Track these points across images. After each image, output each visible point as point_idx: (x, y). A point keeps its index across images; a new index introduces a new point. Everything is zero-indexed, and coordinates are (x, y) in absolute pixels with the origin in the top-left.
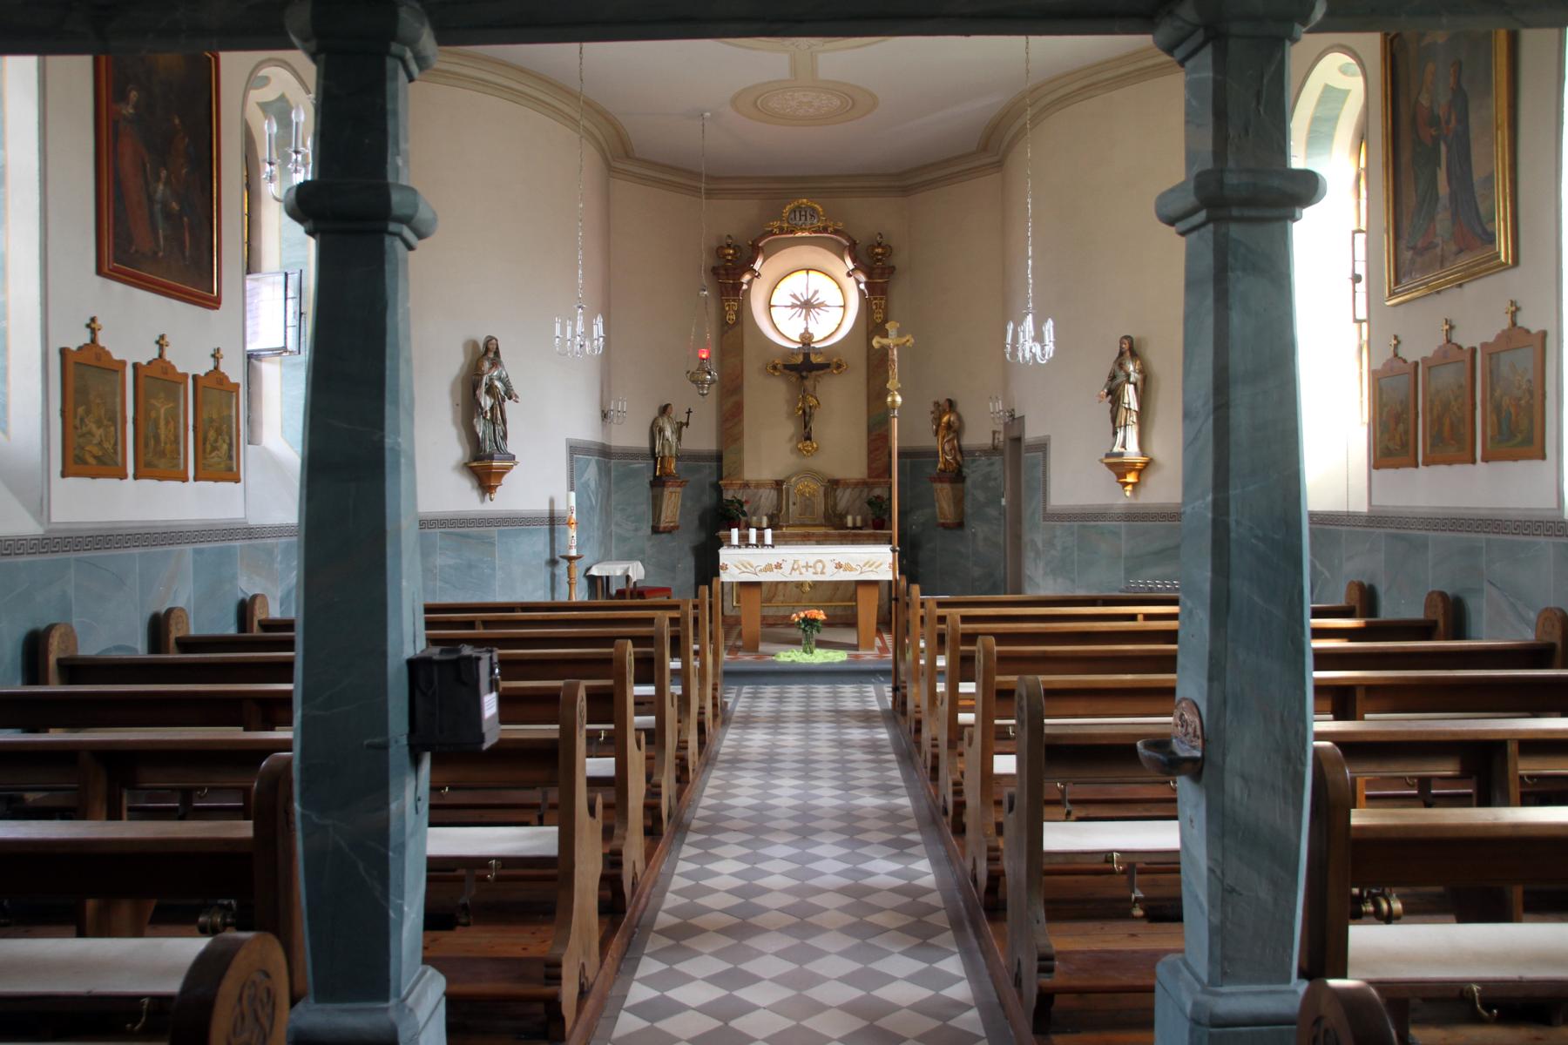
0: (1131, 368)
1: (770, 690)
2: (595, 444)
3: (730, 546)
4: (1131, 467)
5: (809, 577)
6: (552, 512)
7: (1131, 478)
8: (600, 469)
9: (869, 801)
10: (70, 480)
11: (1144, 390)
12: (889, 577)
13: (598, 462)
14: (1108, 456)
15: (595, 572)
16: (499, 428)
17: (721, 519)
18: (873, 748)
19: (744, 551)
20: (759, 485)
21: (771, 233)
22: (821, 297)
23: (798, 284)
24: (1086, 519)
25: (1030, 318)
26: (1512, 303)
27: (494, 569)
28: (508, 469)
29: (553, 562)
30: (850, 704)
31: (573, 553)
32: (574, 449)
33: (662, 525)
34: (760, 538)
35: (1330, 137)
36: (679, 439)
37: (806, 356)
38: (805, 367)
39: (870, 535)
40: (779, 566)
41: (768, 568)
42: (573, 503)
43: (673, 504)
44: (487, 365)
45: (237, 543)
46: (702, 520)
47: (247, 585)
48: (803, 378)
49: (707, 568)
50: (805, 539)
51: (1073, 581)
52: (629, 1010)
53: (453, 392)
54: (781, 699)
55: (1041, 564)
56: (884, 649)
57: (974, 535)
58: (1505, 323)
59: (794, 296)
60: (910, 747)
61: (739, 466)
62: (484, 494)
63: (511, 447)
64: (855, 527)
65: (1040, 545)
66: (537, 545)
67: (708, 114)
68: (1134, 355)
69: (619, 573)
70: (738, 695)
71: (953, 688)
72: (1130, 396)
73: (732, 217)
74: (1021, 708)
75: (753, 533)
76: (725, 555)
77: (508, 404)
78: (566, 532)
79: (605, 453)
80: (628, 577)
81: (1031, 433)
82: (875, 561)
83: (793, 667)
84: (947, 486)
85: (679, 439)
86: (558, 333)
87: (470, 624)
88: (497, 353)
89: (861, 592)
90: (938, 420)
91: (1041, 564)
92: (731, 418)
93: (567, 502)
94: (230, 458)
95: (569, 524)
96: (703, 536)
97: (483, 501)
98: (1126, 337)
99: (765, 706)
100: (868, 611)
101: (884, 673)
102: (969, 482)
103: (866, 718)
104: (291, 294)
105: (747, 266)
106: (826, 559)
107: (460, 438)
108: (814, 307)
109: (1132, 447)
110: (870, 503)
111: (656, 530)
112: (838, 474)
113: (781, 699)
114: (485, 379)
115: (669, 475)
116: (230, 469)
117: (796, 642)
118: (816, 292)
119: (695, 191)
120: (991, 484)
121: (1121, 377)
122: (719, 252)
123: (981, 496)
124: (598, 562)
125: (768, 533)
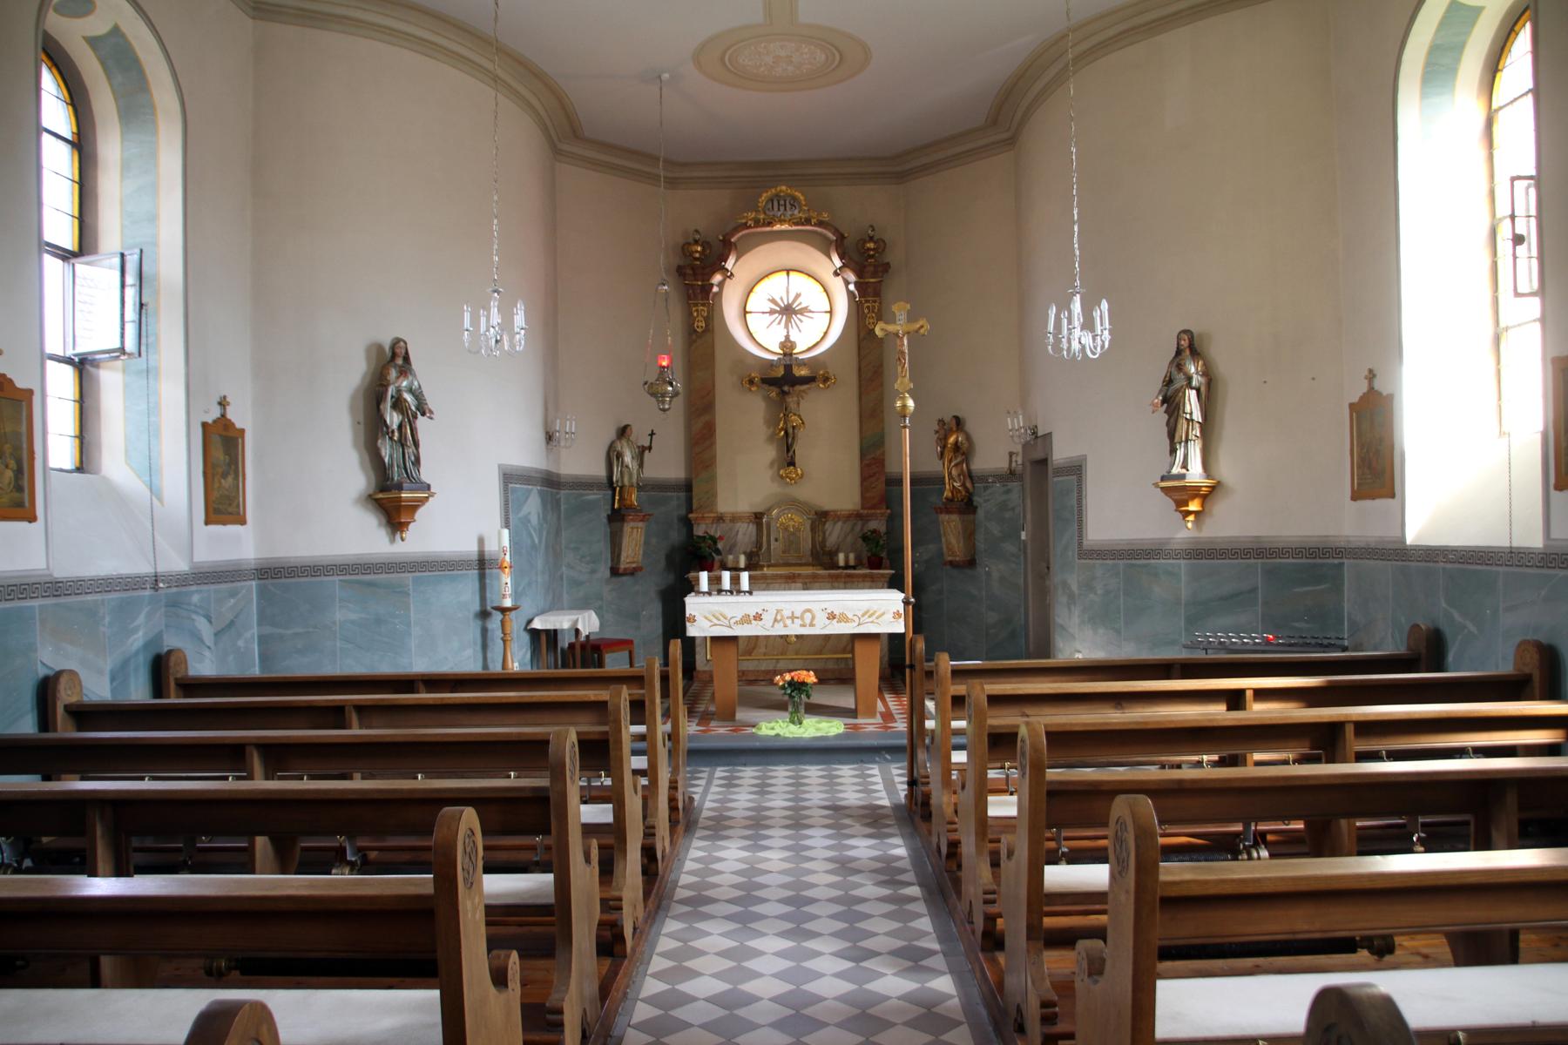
0: (1193, 370)
1: (749, 774)
2: (540, 471)
3: (699, 593)
4: (1194, 492)
5: (794, 629)
6: (481, 554)
7: (1194, 506)
8: (544, 503)
9: (892, 984)
10: (212, 528)
11: (1208, 397)
12: (899, 627)
13: (540, 492)
14: (1163, 479)
15: (537, 624)
16: (410, 450)
17: (692, 556)
18: (887, 872)
19: (715, 599)
20: (735, 518)
21: (745, 226)
22: (804, 302)
23: (776, 287)
24: (1136, 558)
25: (1077, 298)
26: (1371, 371)
27: (409, 625)
28: (424, 500)
29: (484, 615)
30: (851, 797)
31: (508, 603)
32: (510, 478)
33: (622, 566)
34: (735, 581)
35: (1452, 71)
36: (641, 465)
37: (788, 368)
38: (784, 380)
39: (864, 576)
40: (758, 617)
41: (746, 620)
42: (506, 542)
43: (634, 540)
44: (393, 373)
45: (36, 603)
46: (669, 558)
47: (49, 658)
48: (784, 393)
49: (675, 621)
50: (790, 581)
51: (1118, 632)
52: (643, 1000)
53: (352, 409)
54: (763, 788)
55: (1076, 612)
56: (888, 716)
57: (988, 574)
58: (1364, 388)
59: (773, 301)
60: (943, 876)
61: (712, 495)
62: (393, 533)
63: (426, 474)
64: (847, 567)
65: (1074, 587)
66: (465, 593)
67: (666, 76)
68: (1195, 353)
69: (566, 625)
70: (709, 783)
71: (944, 724)
72: (1192, 404)
73: (697, 211)
74: (1023, 754)
75: (726, 575)
76: (693, 604)
77: (421, 422)
78: (498, 579)
79: (551, 482)
80: (577, 631)
81: (1061, 453)
82: (879, 610)
83: (778, 744)
84: (955, 517)
85: (641, 465)
86: (467, 324)
87: (336, 716)
88: (407, 359)
89: (859, 648)
90: (943, 440)
91: (1076, 612)
92: (701, 440)
93: (500, 541)
94: (19, 489)
95: (502, 568)
96: (671, 578)
97: (392, 541)
98: (1185, 332)
99: (743, 800)
100: (869, 666)
101: (894, 750)
102: (981, 513)
103: (873, 819)
104: (130, 280)
105: (717, 264)
106: (816, 608)
107: (362, 464)
108: (796, 312)
109: (1195, 473)
110: (865, 538)
111: (615, 572)
112: (827, 504)
113: (763, 788)
114: (391, 390)
115: (631, 507)
116: (20, 504)
117: (781, 706)
118: (798, 296)
119: (653, 179)
120: (1008, 515)
121: (1180, 380)
122: (685, 249)
123: (995, 529)
124: (542, 612)
125: (745, 577)
